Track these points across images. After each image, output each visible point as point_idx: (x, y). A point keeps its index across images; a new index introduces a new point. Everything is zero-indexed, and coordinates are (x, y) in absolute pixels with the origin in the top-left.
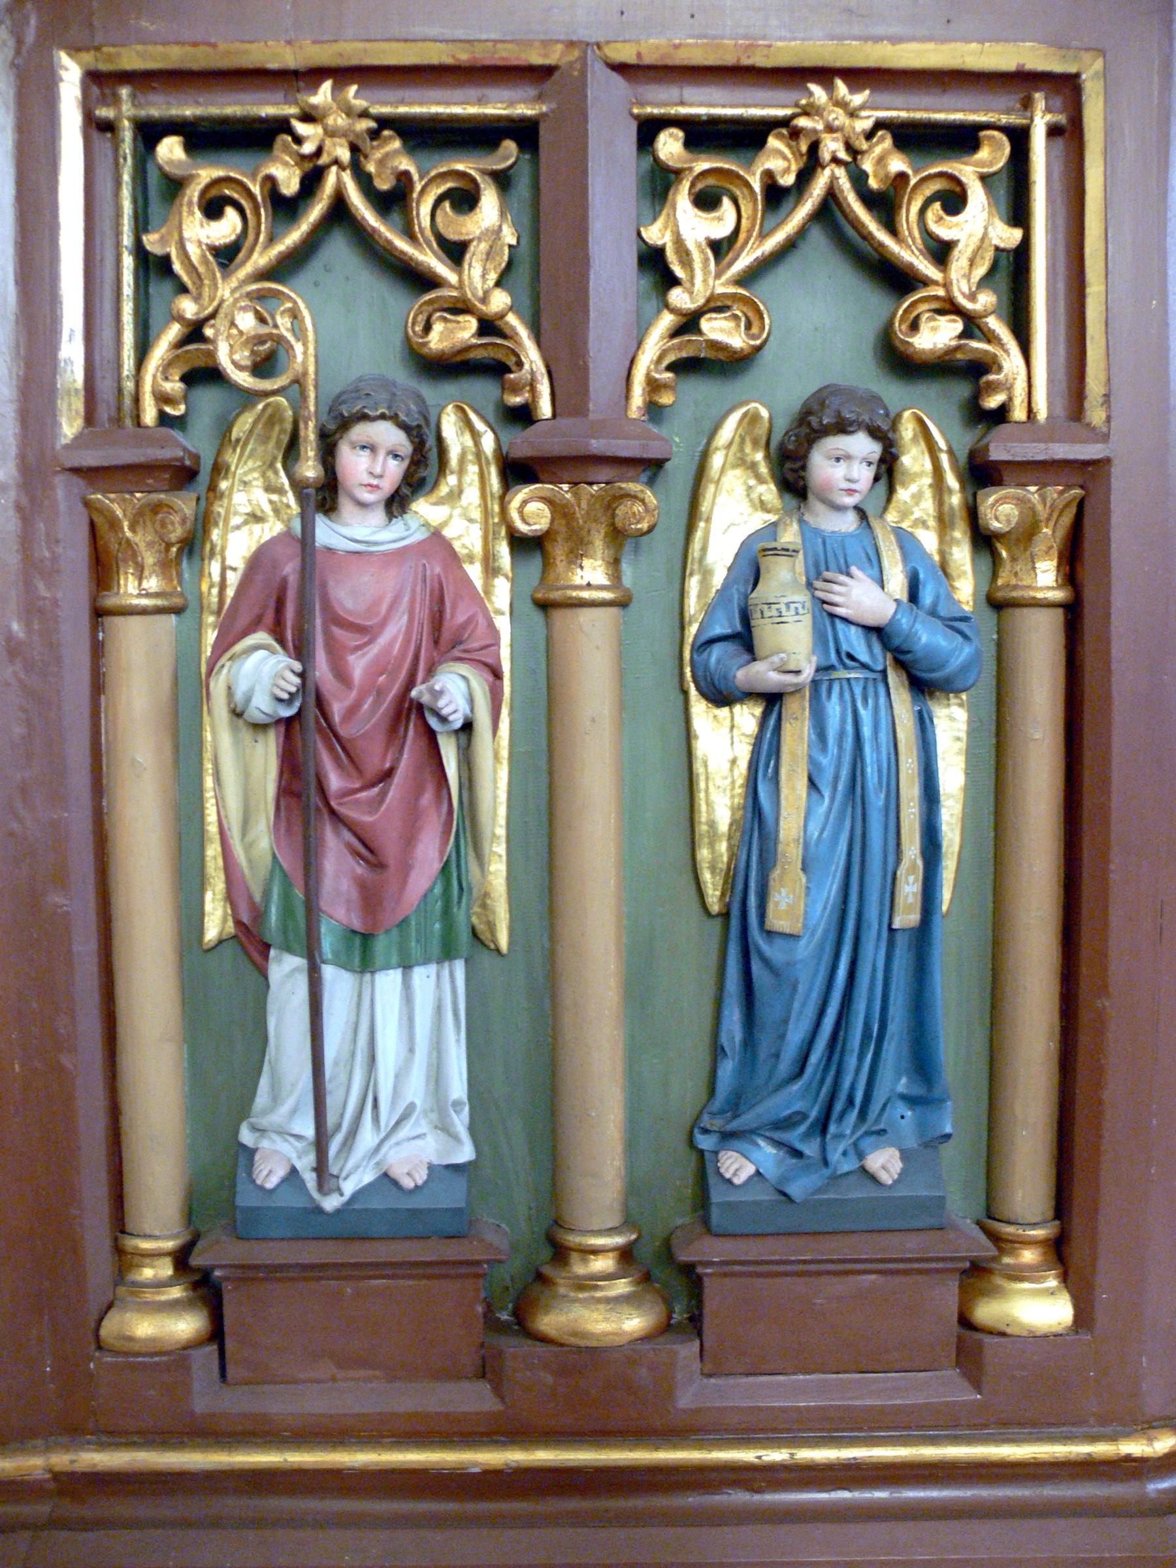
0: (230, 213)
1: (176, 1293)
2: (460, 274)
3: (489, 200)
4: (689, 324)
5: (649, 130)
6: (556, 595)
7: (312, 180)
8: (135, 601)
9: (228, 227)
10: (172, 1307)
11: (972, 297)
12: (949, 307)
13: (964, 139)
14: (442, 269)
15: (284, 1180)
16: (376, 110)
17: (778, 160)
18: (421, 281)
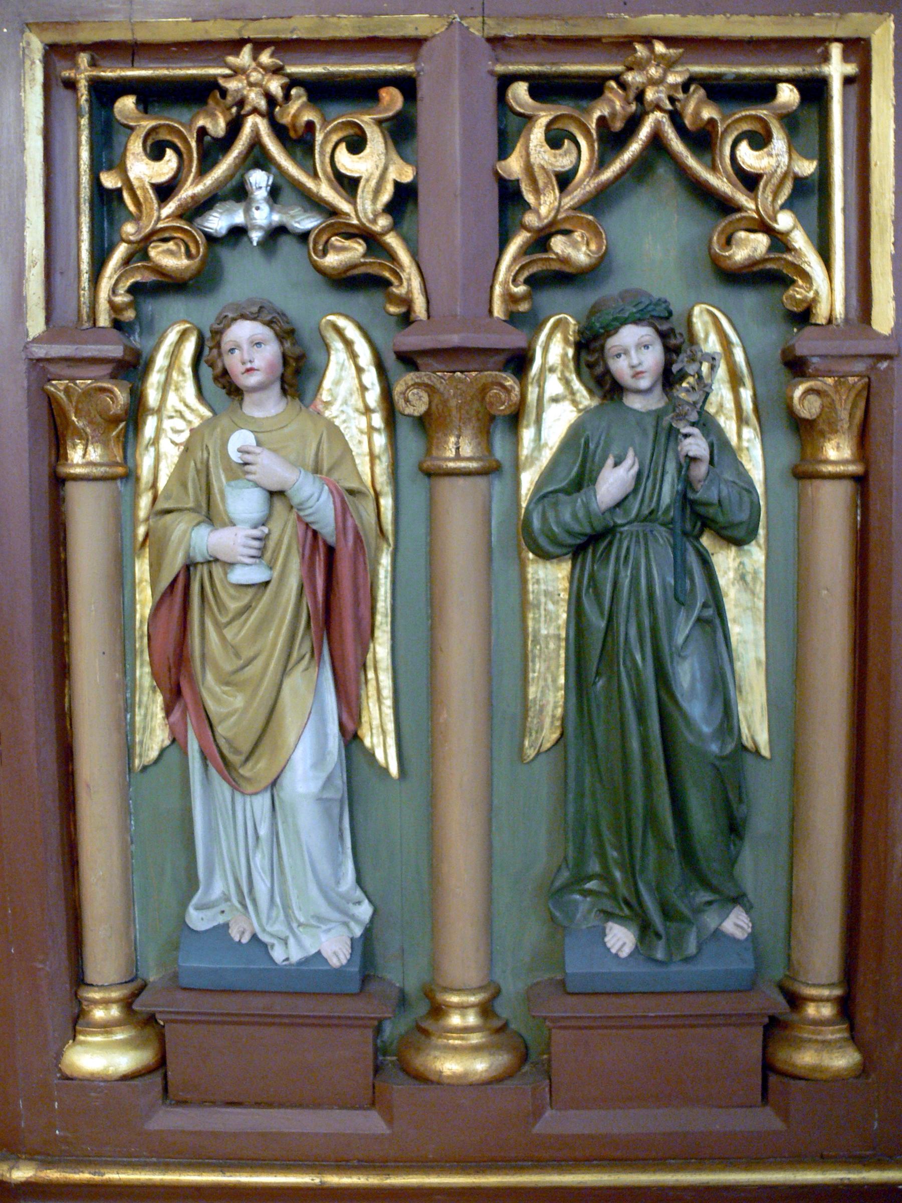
0: (169, 153)
1: (475, 1039)
2: (354, 203)
3: (779, 143)
4: (541, 242)
5: (505, 81)
6: (809, 468)
7: (235, 127)
8: (451, 465)
9: (168, 165)
10: (476, 1049)
11: (374, 221)
12: (763, 227)
13: (364, 91)
14: (742, 198)
15: (250, 941)
16: (290, 69)
17: (612, 105)
18: (725, 207)
